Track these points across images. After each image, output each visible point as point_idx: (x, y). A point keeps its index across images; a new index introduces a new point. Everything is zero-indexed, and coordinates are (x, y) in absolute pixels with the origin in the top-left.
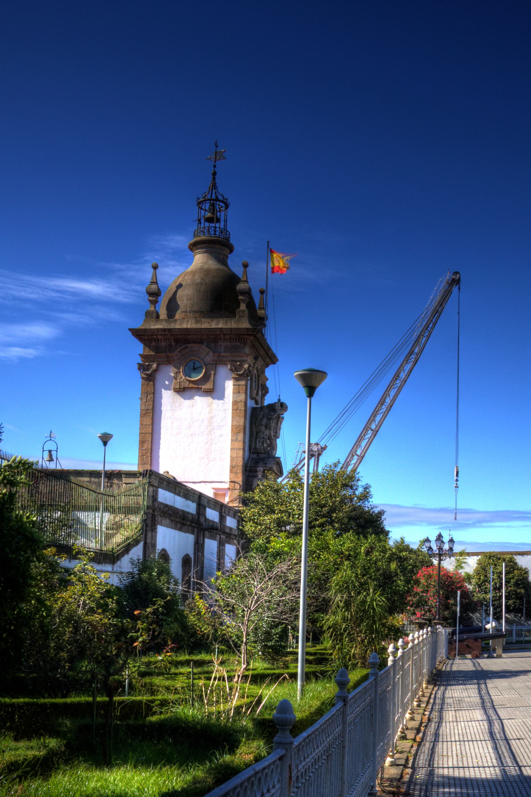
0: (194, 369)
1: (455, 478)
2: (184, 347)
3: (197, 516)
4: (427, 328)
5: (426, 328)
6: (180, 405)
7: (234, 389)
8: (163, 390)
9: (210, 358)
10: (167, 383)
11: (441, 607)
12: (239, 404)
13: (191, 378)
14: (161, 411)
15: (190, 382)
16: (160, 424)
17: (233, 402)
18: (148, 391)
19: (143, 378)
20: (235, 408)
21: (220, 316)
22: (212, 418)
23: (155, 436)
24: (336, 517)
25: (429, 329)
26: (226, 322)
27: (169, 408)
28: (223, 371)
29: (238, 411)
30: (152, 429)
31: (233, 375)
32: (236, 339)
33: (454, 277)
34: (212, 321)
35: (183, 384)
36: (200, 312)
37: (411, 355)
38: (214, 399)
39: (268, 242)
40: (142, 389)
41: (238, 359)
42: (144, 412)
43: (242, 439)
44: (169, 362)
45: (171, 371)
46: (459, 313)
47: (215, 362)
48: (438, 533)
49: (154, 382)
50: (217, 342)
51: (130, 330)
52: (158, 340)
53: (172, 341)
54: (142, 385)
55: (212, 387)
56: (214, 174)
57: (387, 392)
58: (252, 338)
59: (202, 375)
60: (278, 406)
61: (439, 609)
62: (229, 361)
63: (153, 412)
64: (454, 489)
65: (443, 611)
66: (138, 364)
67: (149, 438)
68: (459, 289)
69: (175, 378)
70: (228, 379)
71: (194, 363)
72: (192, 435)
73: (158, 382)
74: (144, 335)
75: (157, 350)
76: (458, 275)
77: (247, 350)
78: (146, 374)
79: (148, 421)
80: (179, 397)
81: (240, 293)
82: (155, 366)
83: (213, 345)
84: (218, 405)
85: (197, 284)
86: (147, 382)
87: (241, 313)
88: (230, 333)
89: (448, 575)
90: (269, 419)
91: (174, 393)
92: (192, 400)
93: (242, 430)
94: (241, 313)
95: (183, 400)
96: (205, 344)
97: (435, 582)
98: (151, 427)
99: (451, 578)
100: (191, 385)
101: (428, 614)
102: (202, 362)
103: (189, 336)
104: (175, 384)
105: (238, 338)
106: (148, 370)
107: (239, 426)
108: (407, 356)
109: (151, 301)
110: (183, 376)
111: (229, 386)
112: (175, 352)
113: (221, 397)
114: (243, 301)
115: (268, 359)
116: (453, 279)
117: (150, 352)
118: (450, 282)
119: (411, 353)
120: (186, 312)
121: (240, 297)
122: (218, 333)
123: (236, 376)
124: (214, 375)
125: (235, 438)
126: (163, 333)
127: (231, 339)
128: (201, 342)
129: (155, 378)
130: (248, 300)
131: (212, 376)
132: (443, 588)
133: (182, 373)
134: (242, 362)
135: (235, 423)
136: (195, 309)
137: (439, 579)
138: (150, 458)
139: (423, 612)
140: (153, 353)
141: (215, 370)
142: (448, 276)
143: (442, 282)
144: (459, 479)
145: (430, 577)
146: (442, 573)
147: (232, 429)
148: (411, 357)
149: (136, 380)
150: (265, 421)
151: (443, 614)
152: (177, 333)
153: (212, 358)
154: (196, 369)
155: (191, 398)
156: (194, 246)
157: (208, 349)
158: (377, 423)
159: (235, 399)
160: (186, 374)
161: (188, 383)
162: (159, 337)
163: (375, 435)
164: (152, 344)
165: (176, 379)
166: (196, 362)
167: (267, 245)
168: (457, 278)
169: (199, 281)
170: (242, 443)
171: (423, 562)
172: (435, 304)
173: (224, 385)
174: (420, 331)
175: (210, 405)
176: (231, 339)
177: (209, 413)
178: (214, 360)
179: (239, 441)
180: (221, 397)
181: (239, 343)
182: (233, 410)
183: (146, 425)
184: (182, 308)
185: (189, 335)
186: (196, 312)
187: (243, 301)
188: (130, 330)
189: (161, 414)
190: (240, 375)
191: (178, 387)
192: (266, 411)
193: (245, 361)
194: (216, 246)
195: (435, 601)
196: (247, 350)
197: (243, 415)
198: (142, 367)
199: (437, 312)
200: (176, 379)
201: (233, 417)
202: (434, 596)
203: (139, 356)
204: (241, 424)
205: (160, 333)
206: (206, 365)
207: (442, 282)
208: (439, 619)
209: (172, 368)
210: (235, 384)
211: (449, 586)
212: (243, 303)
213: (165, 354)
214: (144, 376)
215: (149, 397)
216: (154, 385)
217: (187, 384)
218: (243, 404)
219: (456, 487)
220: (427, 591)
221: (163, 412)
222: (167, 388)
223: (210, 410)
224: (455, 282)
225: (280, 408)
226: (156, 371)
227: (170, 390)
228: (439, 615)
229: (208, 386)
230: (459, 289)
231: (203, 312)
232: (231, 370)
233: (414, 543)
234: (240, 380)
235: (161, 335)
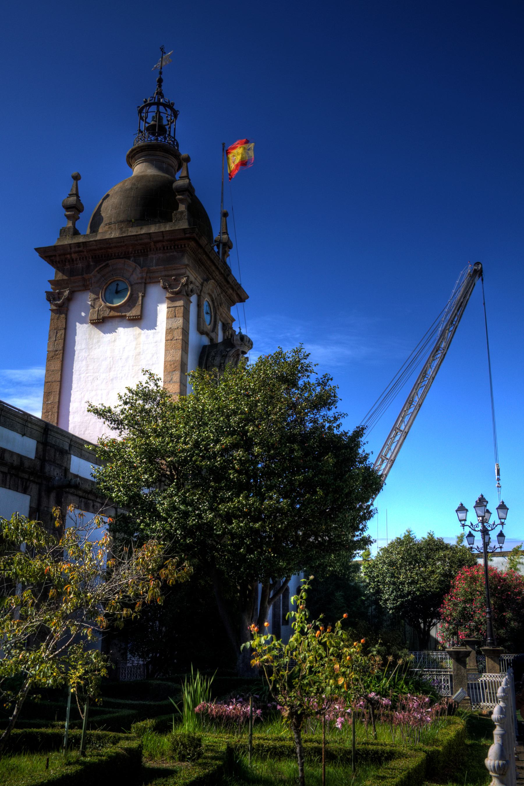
0: (117, 292)
1: (497, 477)
2: (104, 264)
3: (38, 463)
4: (452, 321)
5: (451, 322)
6: (98, 342)
7: (168, 312)
8: (77, 324)
9: (137, 276)
10: (83, 314)
11: (493, 623)
12: (175, 332)
13: (113, 304)
14: (74, 351)
15: (111, 309)
16: (73, 369)
17: (167, 330)
18: (58, 327)
19: (52, 310)
20: (169, 338)
21: (155, 223)
22: (139, 354)
23: (65, 385)
24: (256, 434)
25: (454, 323)
27: (83, 346)
28: (155, 291)
29: (174, 342)
30: (61, 375)
31: (168, 295)
32: (171, 247)
33: (476, 268)
34: (141, 229)
35: (101, 313)
36: (128, 221)
37: (437, 351)
38: (142, 329)
39: (223, 144)
40: (51, 324)
41: (174, 272)
42: (52, 354)
43: (178, 380)
44: (85, 288)
45: (88, 298)
46: (484, 304)
47: (144, 281)
48: (479, 496)
49: (66, 315)
51: (36, 249)
52: (73, 260)
53: (90, 260)
55: (139, 313)
56: (160, 81)
57: (414, 391)
58: (192, 244)
59: (126, 299)
60: (237, 340)
61: (491, 624)
62: (161, 276)
63: (63, 353)
64: (496, 489)
65: (498, 629)
66: (46, 292)
67: (56, 387)
68: (482, 280)
69: (93, 307)
70: (162, 302)
71: (117, 285)
72: (112, 380)
73: (72, 316)
74: (55, 256)
75: (71, 273)
76: (480, 266)
77: (186, 261)
78: (56, 305)
79: (57, 365)
80: (98, 330)
81: (178, 192)
82: (67, 293)
83: (142, 259)
84: (147, 337)
85: (126, 190)
86: (58, 315)
87: (178, 216)
88: (161, 238)
89: (497, 576)
90: (224, 357)
91: (91, 326)
92: (114, 333)
93: (179, 367)
94: (178, 216)
95: (102, 334)
96: (132, 259)
97: (481, 586)
98: (60, 373)
99: (505, 580)
100: (113, 313)
101: (475, 633)
102: (126, 281)
103: (110, 250)
104: (93, 314)
105: (174, 244)
106: (59, 299)
107: (175, 362)
108: (432, 352)
109: (68, 217)
110: (103, 303)
111: (162, 310)
112: (93, 273)
113: (152, 326)
114: (182, 201)
115: (231, 291)
116: (475, 270)
117: (60, 276)
118: (471, 273)
119: (437, 349)
120: (110, 224)
121: (178, 197)
122: (146, 241)
123: (171, 295)
124: (143, 297)
126: (77, 249)
127: (164, 248)
128: (127, 256)
129: (67, 310)
130: (190, 201)
131: (140, 298)
132: (493, 595)
133: (101, 300)
134: (179, 276)
135: (169, 358)
136: (121, 219)
137: (487, 582)
138: (56, 415)
139: (468, 631)
140: (65, 278)
141: (145, 291)
142: (469, 269)
143: (463, 275)
144: (501, 477)
145: (474, 579)
146: (490, 573)
147: (165, 367)
148: (437, 353)
149: (45, 313)
150: (218, 360)
151: (498, 634)
152: (95, 247)
153: (140, 275)
154: (118, 293)
155: (112, 330)
156: (133, 157)
157: (134, 264)
158: (406, 423)
159: (170, 326)
160: (106, 300)
161: (108, 311)
162: (74, 256)
163: (406, 437)
164: (66, 267)
165: (94, 308)
166: (120, 283)
167: (221, 146)
168: (479, 268)
169: (129, 187)
170: (179, 384)
171: (463, 560)
172: (459, 295)
173: (156, 310)
174: (445, 324)
175: (137, 338)
176: (164, 248)
177: (136, 348)
178: (142, 278)
179: (175, 382)
180: (152, 326)
181: (175, 253)
182: (166, 340)
183: (53, 371)
184: (106, 220)
185: (111, 248)
186: (121, 222)
187: (182, 201)
188: (36, 249)
189: (74, 355)
190: (177, 293)
191: (95, 317)
192: (222, 348)
193: (183, 275)
194: (158, 153)
195: (483, 614)
196: (186, 261)
197: (180, 346)
198: (51, 297)
199: (461, 306)
200: (94, 308)
201: (166, 350)
202: (482, 607)
203: (49, 283)
204: (177, 359)
205: (73, 250)
206: (131, 285)
207: (463, 275)
208: (492, 644)
209: (90, 294)
210: (169, 306)
211: (502, 592)
212: (182, 203)
213: (80, 277)
214: (55, 308)
215: (58, 335)
216: (66, 319)
217: (107, 313)
218: (180, 331)
219: (498, 487)
220: (472, 600)
221: (76, 353)
222: (83, 321)
223: (137, 344)
224: (478, 273)
225: (239, 342)
226: (69, 299)
227: (86, 323)
228: (491, 636)
229: (135, 312)
230: (482, 280)
231: (131, 221)
232: (165, 288)
233: (452, 539)
234: (176, 301)
235: (75, 252)
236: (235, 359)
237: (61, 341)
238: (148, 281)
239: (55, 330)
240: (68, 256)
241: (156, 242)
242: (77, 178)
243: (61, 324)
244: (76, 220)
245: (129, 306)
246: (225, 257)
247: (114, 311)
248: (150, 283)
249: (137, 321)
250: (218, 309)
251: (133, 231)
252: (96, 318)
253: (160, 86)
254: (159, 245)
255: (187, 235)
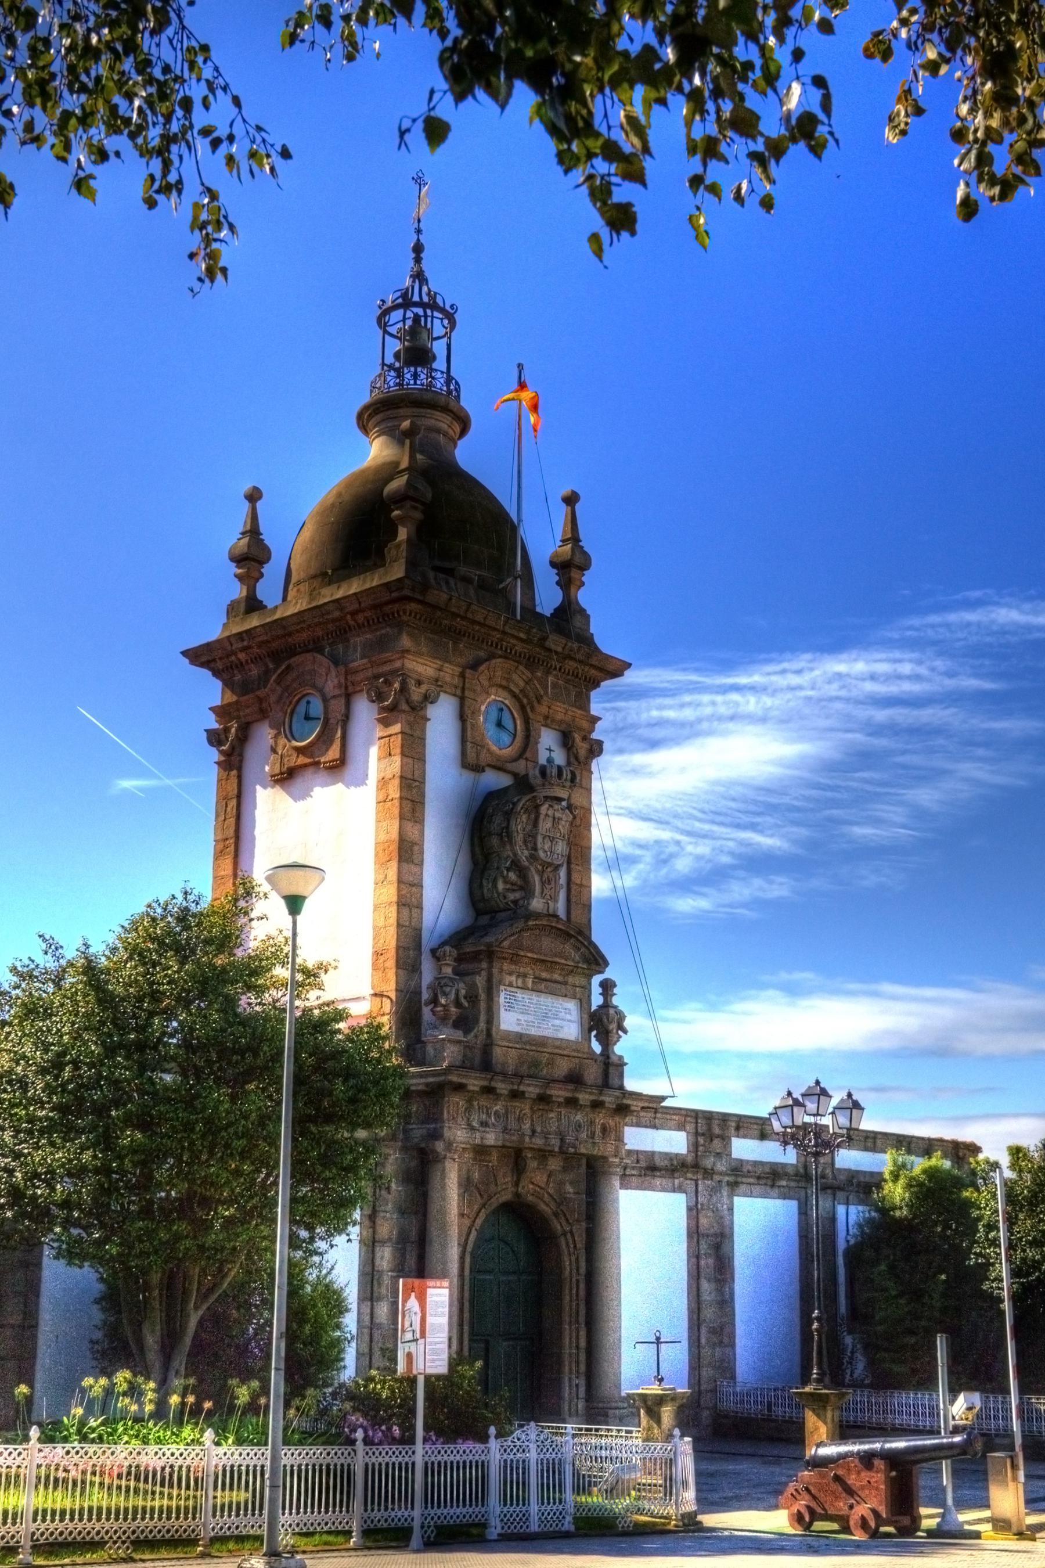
8: (258, 787)
15: (299, 750)
26: (364, 582)
42: (221, 846)
50: (348, 641)
51: (184, 653)
54: (219, 781)
56: (418, 249)
74: (214, 660)
77: (406, 642)
94: (394, 552)
100: (302, 760)
114: (402, 519)
125: (382, 877)
136: (312, 572)
162: (242, 656)
178: (340, 686)
186: (314, 577)
187: (402, 519)
188: (184, 653)
196: (406, 642)
198: (215, 738)
218: (397, 782)
236: (533, 816)
237: (233, 820)
238: (351, 689)
239: (223, 800)
240: (233, 658)
241: (353, 614)
242: (254, 496)
243: (232, 787)
244: (257, 580)
245: (324, 742)
246: (573, 590)
247: (304, 754)
248: (355, 692)
249: (338, 768)
250: (533, 708)
251: (330, 594)
252: (277, 771)
253: (418, 260)
254: (360, 618)
255: (395, 595)
